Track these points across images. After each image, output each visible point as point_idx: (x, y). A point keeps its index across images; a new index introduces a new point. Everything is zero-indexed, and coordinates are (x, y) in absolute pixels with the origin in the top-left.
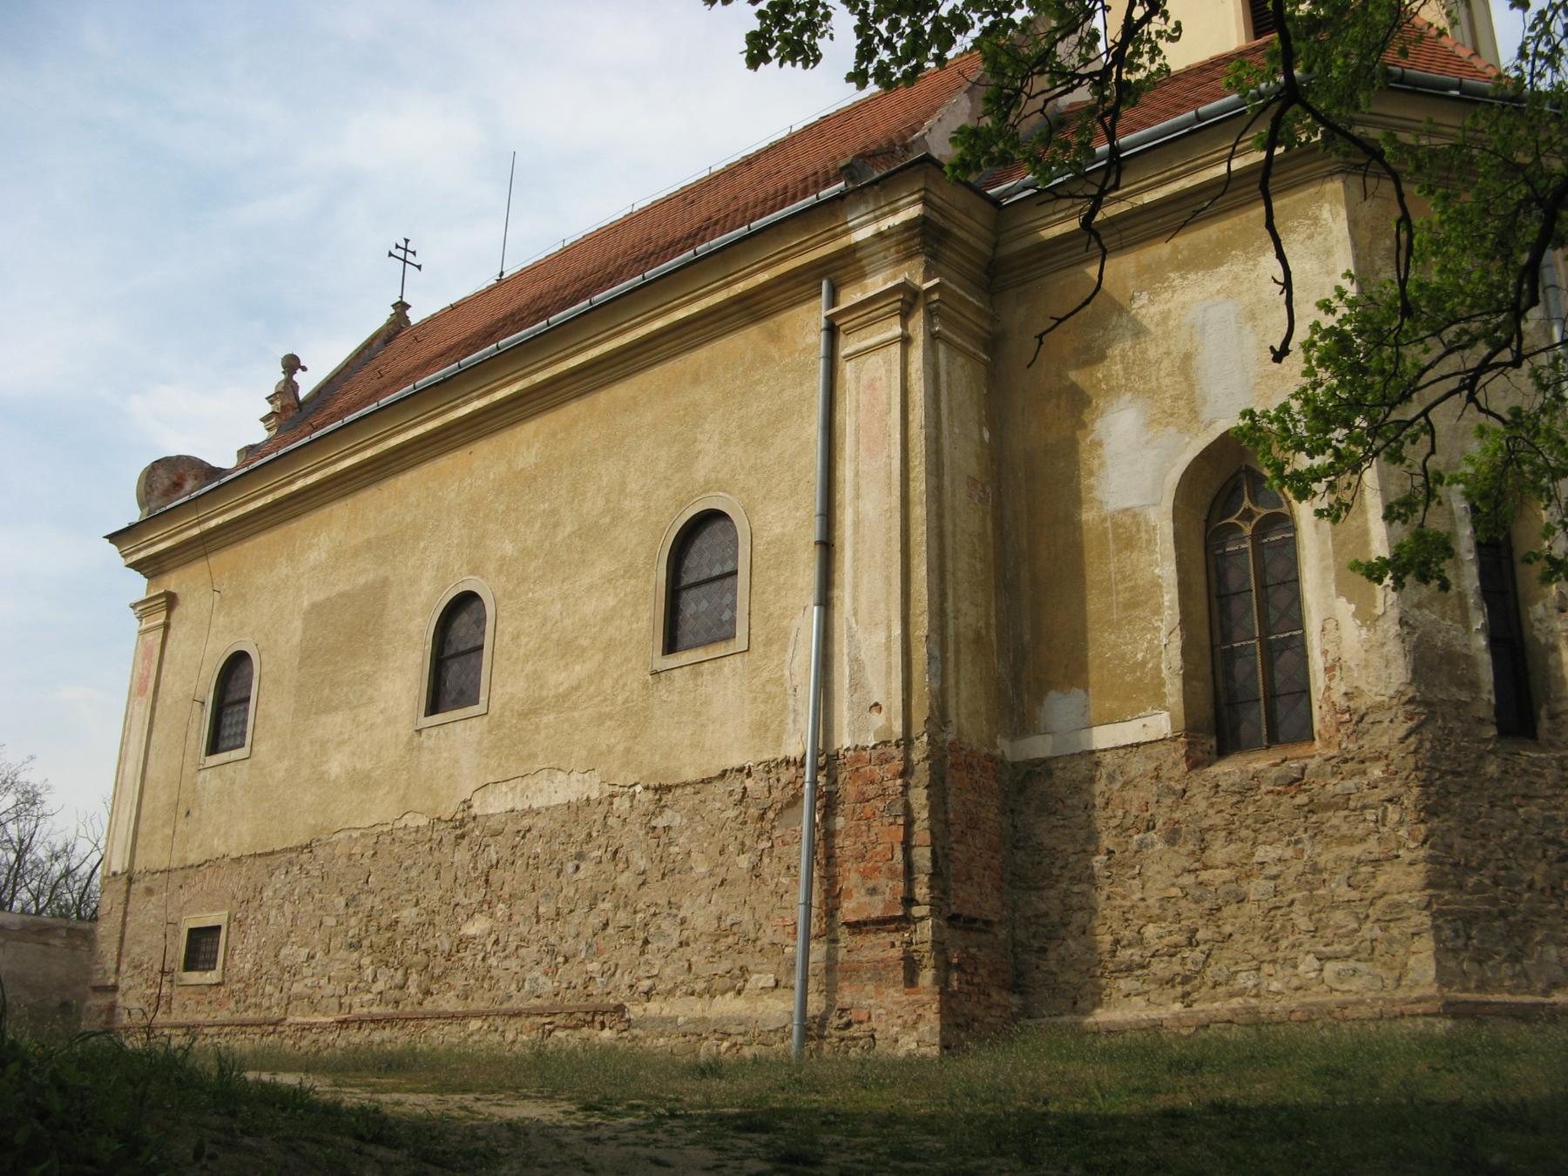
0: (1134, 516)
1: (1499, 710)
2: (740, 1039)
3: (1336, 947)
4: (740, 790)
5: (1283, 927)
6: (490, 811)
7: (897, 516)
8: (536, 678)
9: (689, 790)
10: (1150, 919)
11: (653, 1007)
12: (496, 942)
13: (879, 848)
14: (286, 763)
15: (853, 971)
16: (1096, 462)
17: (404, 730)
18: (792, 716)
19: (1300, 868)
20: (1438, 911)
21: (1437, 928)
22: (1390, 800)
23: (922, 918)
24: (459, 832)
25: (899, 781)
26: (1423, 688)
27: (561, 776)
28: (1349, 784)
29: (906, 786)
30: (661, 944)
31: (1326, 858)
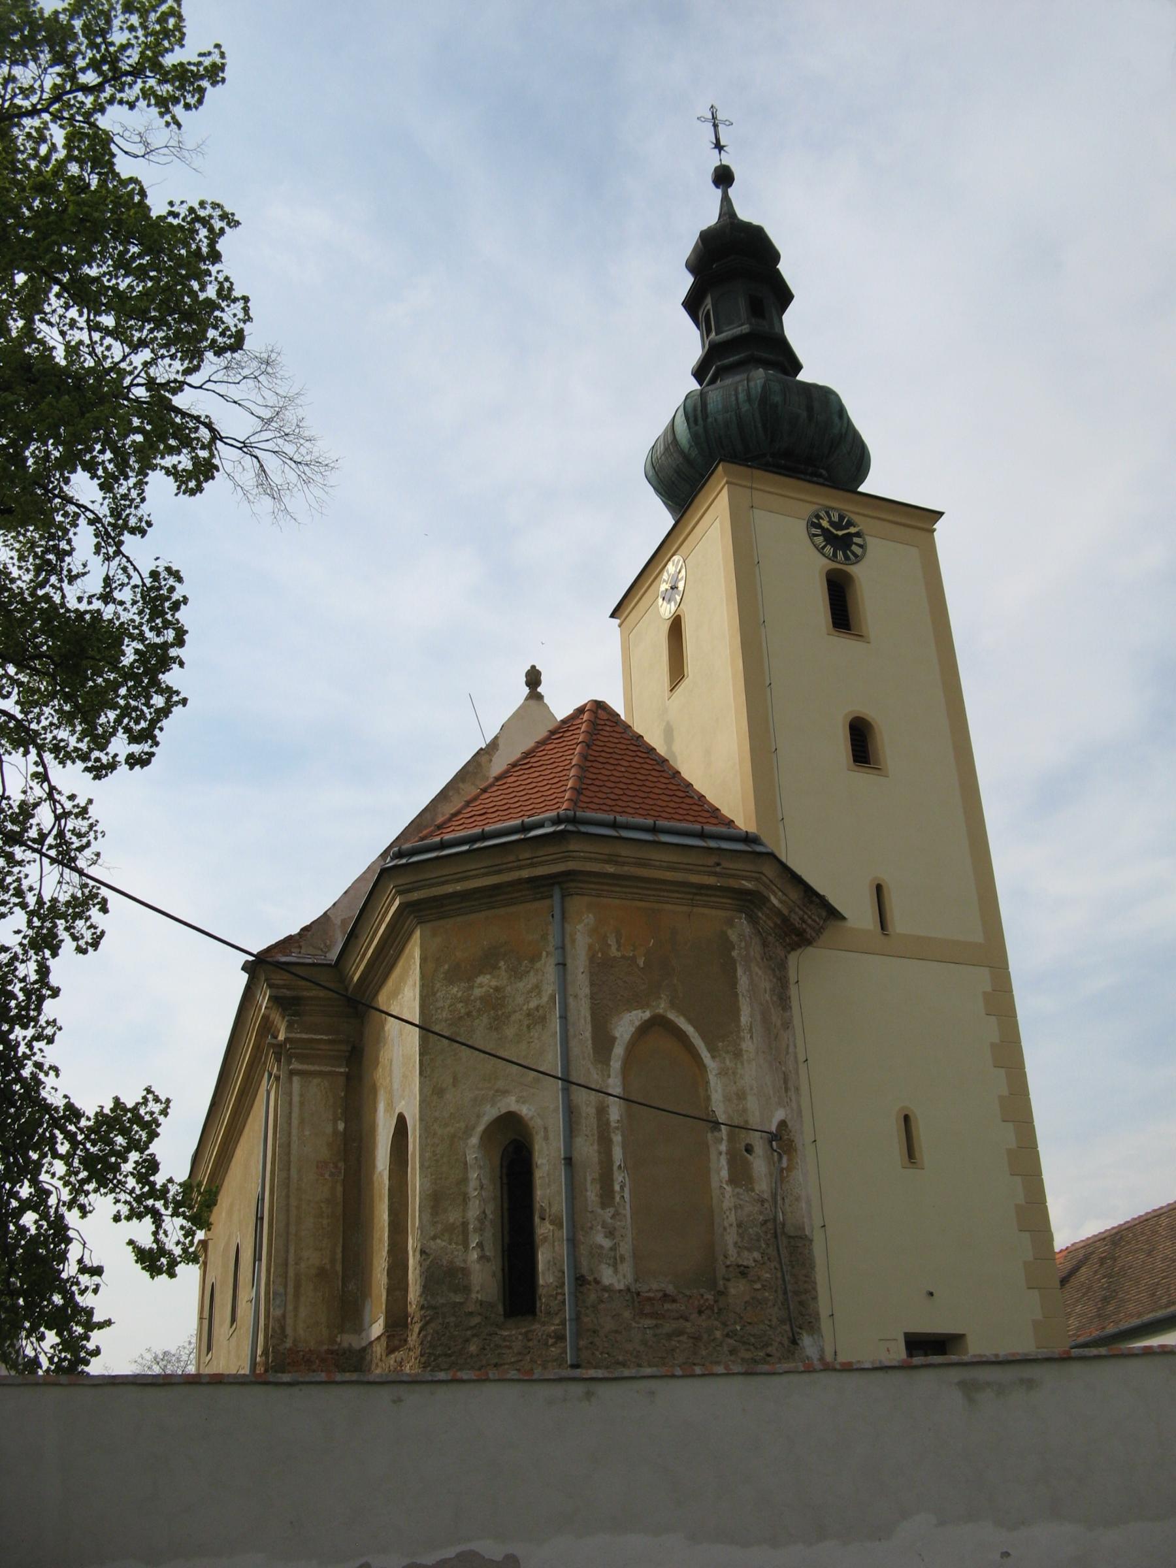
26: (429, 1298)
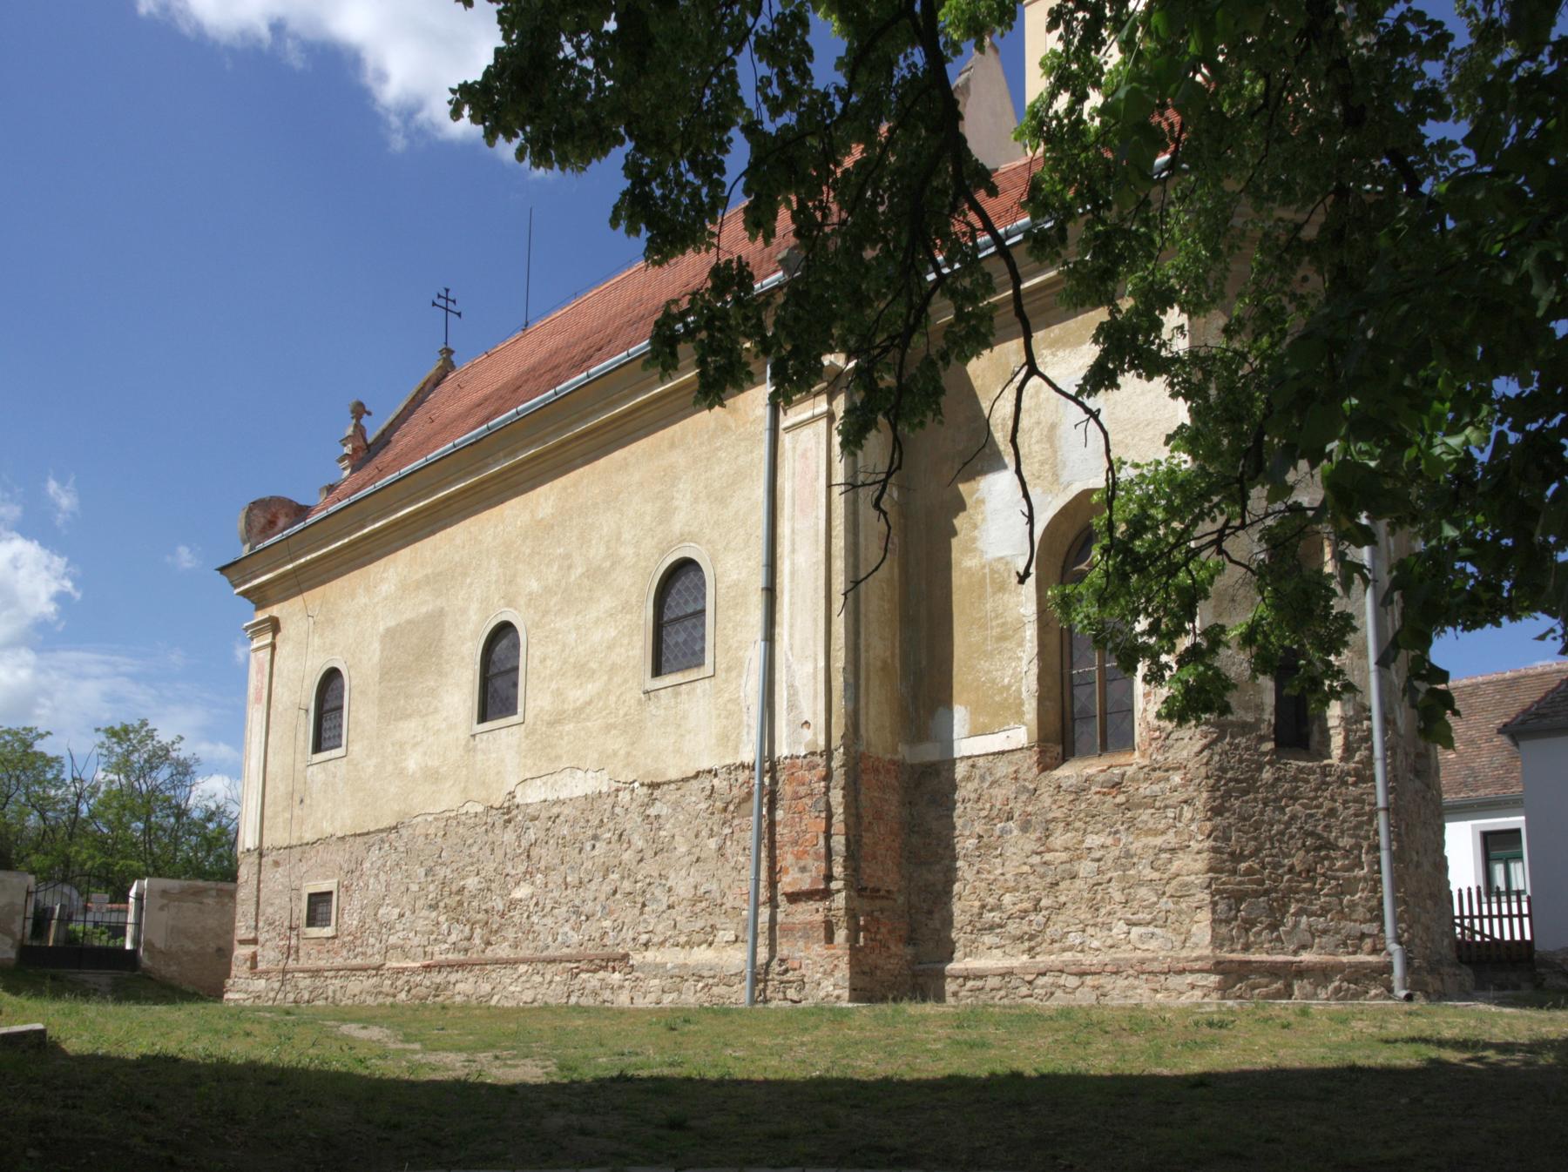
0: (1007, 563)
1: (1278, 729)
2: (711, 981)
3: (1140, 916)
4: (709, 787)
5: (1103, 899)
6: (529, 801)
7: (823, 568)
8: (558, 693)
9: (673, 786)
10: (1008, 890)
11: (650, 955)
12: (537, 904)
13: (808, 836)
14: (374, 761)
15: (789, 930)
16: (980, 517)
17: (462, 734)
18: (746, 730)
19: (1117, 853)
20: (1216, 890)
21: (1214, 904)
22: (1185, 802)
23: (839, 891)
24: (506, 817)
25: (822, 784)
27: (580, 774)
28: (1156, 788)
29: (828, 789)
30: (655, 907)
31: (1136, 846)
